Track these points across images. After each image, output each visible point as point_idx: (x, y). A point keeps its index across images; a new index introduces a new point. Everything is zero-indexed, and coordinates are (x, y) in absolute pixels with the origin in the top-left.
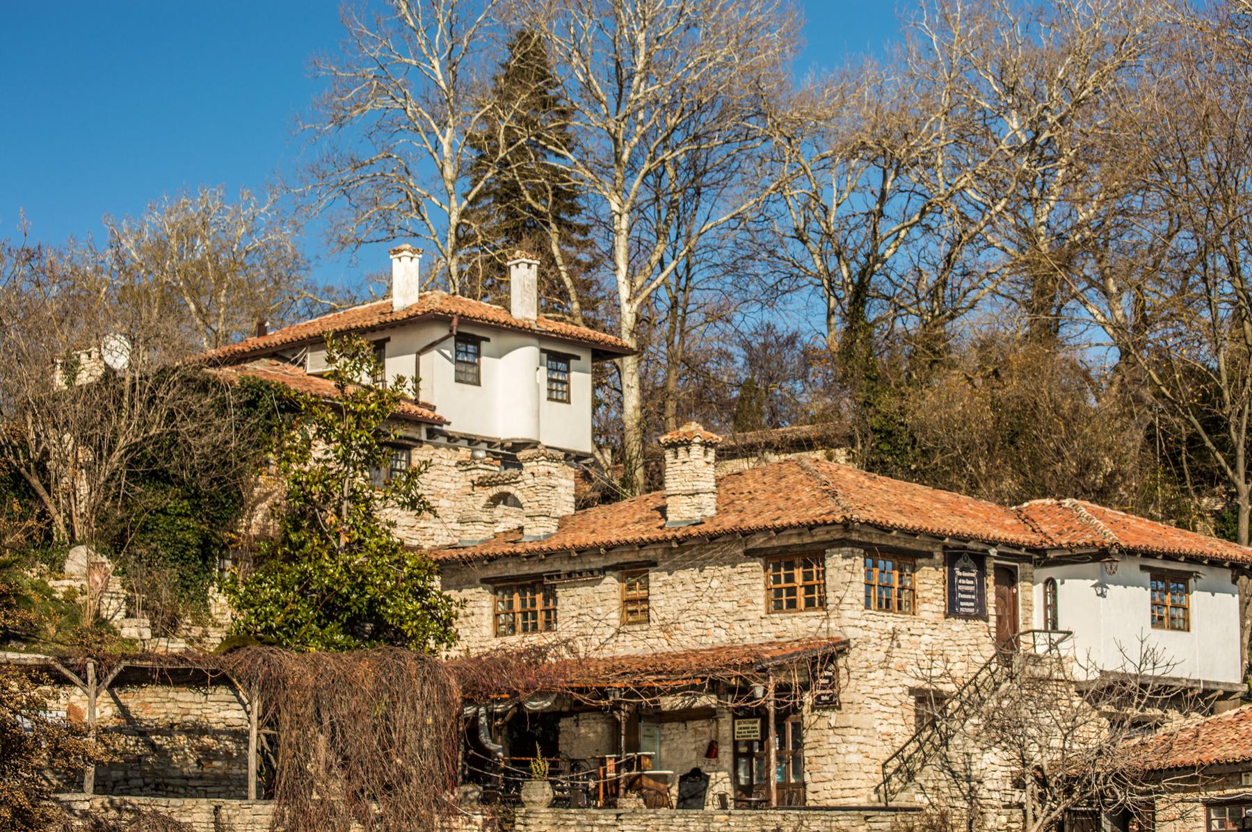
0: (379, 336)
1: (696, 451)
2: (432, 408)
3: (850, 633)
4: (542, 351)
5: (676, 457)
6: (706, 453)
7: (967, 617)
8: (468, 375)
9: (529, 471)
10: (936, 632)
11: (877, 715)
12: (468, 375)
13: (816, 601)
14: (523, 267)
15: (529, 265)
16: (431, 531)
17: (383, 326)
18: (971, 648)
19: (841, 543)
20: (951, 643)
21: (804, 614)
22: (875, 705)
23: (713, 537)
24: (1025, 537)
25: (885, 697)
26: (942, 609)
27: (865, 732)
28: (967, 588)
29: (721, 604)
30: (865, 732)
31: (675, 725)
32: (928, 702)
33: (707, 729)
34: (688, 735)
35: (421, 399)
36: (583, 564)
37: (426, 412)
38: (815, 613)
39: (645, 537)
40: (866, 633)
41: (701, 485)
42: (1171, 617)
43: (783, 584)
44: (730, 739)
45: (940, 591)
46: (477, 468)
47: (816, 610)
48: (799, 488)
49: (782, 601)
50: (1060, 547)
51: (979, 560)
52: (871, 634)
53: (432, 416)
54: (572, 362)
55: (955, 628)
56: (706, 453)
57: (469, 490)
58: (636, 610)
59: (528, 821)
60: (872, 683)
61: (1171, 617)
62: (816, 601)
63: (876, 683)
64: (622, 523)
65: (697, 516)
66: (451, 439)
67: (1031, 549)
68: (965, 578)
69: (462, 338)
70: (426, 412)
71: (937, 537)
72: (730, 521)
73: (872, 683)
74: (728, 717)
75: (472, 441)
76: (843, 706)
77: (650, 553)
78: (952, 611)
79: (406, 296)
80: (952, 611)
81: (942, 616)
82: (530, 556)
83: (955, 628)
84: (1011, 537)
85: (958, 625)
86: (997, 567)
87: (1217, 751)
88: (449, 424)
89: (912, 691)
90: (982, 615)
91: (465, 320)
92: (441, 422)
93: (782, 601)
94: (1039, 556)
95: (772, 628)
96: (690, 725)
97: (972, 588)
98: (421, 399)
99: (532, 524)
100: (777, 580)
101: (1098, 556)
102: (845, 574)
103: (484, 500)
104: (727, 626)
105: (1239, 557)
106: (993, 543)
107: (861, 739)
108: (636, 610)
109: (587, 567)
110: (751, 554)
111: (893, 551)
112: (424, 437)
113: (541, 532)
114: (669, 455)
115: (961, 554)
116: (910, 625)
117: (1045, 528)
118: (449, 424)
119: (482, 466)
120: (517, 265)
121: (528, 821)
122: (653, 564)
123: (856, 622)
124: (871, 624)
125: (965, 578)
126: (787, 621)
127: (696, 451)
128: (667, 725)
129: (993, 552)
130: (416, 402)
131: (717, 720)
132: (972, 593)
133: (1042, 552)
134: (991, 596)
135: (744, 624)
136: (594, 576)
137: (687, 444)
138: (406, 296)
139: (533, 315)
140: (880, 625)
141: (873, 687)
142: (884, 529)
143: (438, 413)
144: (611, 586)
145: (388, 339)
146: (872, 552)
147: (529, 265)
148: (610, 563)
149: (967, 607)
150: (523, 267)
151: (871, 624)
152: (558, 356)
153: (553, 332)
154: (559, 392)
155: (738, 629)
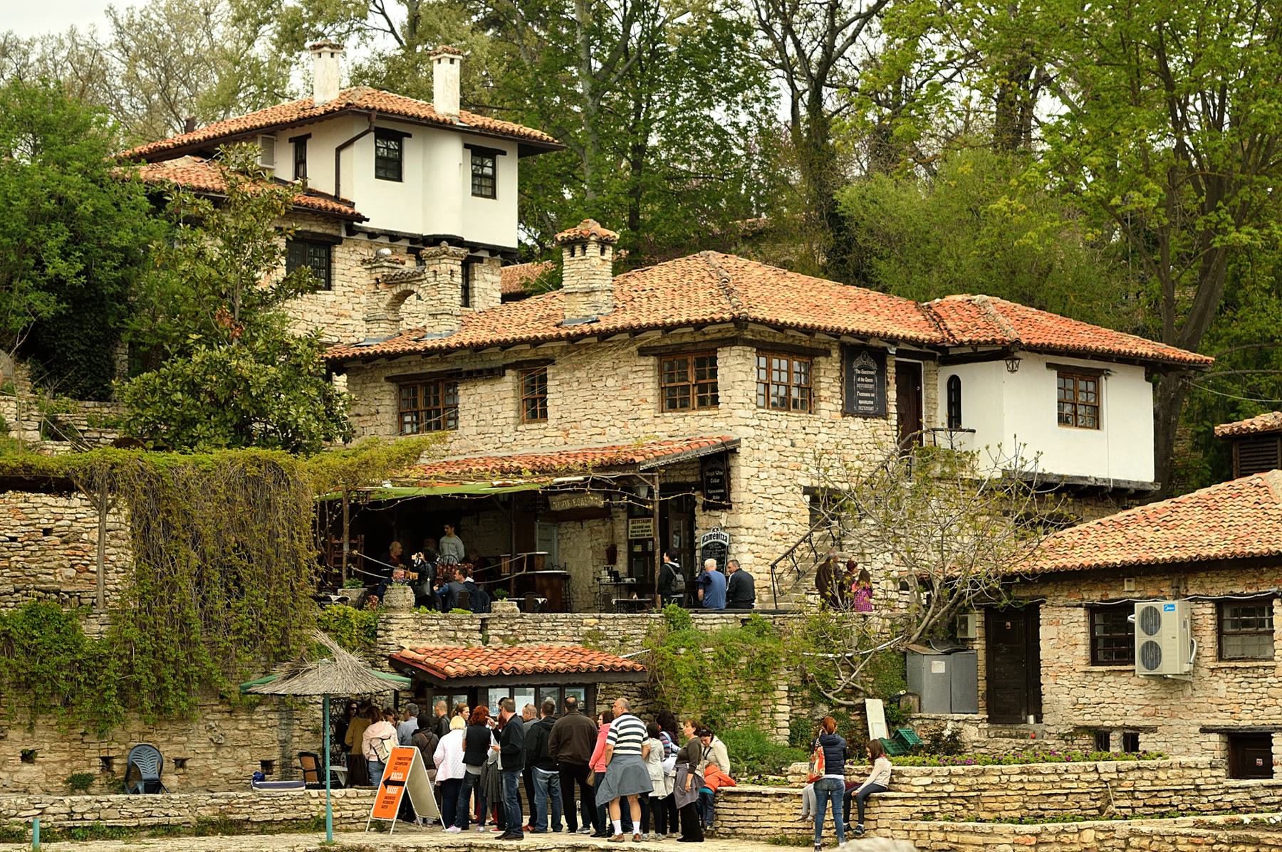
0: (299, 132)
1: (593, 250)
2: (352, 205)
3: (741, 432)
4: (466, 146)
5: (573, 255)
6: (603, 252)
7: (865, 416)
8: (390, 168)
9: (432, 269)
10: (834, 431)
11: (770, 514)
12: (390, 168)
13: (709, 398)
14: (445, 63)
15: (452, 61)
16: (352, 328)
17: (301, 122)
18: (871, 447)
19: (732, 342)
20: (849, 442)
21: (695, 413)
22: (768, 504)
23: (604, 336)
24: (925, 333)
25: (778, 497)
26: (840, 408)
27: (756, 532)
28: (866, 386)
29: (617, 403)
30: (756, 532)
31: (571, 524)
32: (824, 503)
33: (602, 528)
34: (585, 534)
35: (342, 196)
36: (478, 363)
37: (344, 208)
38: (707, 412)
39: (539, 335)
40: (758, 432)
41: (597, 284)
42: (1080, 411)
43: (537, 395)
44: (624, 538)
45: (838, 389)
46: (382, 267)
47: (709, 409)
48: (680, 291)
49: (673, 400)
50: (962, 344)
51: (879, 356)
52: (763, 433)
53: (350, 211)
54: (499, 157)
55: (853, 427)
56: (603, 252)
57: (372, 288)
58: (534, 408)
59: (389, 627)
60: (764, 483)
61: (1080, 411)
62: (709, 398)
63: (768, 483)
64: (524, 322)
65: (593, 314)
66: (372, 235)
67: (932, 345)
68: (864, 376)
69: (381, 134)
70: (344, 208)
71: (836, 333)
72: (622, 320)
73: (764, 483)
74: (623, 516)
75: (393, 237)
76: (734, 506)
77: (545, 350)
78: (849, 410)
79: (326, 92)
80: (849, 410)
81: (839, 414)
82: (429, 352)
83: (853, 427)
84: (911, 333)
85: (857, 424)
86: (898, 365)
87: (1101, 555)
88: (367, 220)
89: (807, 491)
90: (885, 416)
91: (384, 114)
92: (361, 219)
93: (673, 400)
94: (946, 354)
95: (665, 427)
96: (586, 524)
97: (871, 386)
98: (342, 196)
99: (434, 322)
100: (769, 369)
101: (1003, 352)
102: (737, 372)
103: (389, 297)
104: (622, 424)
105: (1150, 354)
106: (894, 340)
107: (753, 539)
108: (534, 408)
109: (487, 366)
110: (643, 352)
111: (790, 346)
112: (344, 235)
113: (444, 329)
114: (566, 254)
115: (860, 351)
116: (805, 424)
117: (950, 325)
118: (367, 220)
119: (386, 264)
120: (439, 60)
121: (389, 627)
122: (551, 361)
123: (748, 422)
124: (764, 423)
125: (864, 376)
126: (680, 420)
127: (593, 250)
128: (564, 524)
129: (893, 351)
130: (336, 198)
131: (611, 519)
132: (871, 392)
133: (944, 349)
134: (892, 394)
135: (637, 422)
136: (494, 374)
137: (583, 242)
138: (326, 92)
139: (456, 110)
140: (774, 424)
141: (766, 487)
142: (781, 328)
143: (357, 209)
144: (509, 385)
145: (309, 136)
146: (765, 348)
147: (452, 61)
148: (509, 361)
149: (866, 404)
150: (445, 63)
151: (764, 423)
152: (482, 151)
153: (476, 126)
154: (484, 186)
155: (632, 428)
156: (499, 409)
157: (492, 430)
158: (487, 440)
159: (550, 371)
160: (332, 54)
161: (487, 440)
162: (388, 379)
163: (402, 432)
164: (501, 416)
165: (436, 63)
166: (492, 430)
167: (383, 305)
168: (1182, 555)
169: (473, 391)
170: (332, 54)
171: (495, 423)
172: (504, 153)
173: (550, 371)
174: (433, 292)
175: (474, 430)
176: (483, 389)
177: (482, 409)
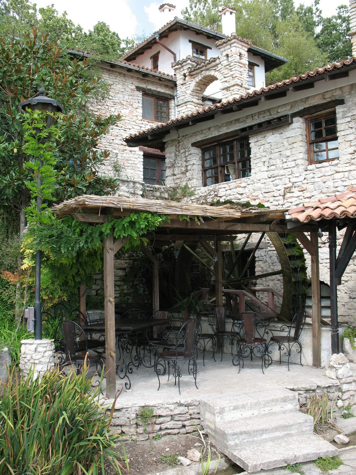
14: (228, 14)
54: (256, 67)
145: (159, 52)
147: (231, 13)
150: (228, 14)
156: (288, 153)
157: (282, 172)
158: (277, 182)
159: (339, 110)
160: (170, 11)
161: (277, 182)
162: (194, 145)
163: (205, 185)
164: (290, 159)
165: (223, 16)
166: (282, 172)
167: (189, 92)
168: (320, 275)
169: (263, 142)
170: (170, 11)
171: (285, 166)
172: (258, 66)
173: (339, 110)
174: (226, 71)
175: (266, 175)
176: (272, 138)
177: (272, 156)
